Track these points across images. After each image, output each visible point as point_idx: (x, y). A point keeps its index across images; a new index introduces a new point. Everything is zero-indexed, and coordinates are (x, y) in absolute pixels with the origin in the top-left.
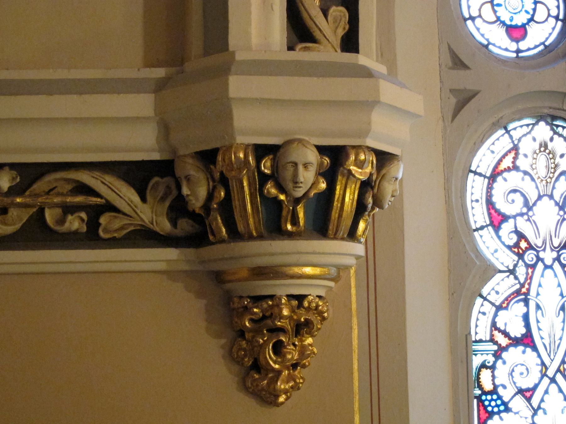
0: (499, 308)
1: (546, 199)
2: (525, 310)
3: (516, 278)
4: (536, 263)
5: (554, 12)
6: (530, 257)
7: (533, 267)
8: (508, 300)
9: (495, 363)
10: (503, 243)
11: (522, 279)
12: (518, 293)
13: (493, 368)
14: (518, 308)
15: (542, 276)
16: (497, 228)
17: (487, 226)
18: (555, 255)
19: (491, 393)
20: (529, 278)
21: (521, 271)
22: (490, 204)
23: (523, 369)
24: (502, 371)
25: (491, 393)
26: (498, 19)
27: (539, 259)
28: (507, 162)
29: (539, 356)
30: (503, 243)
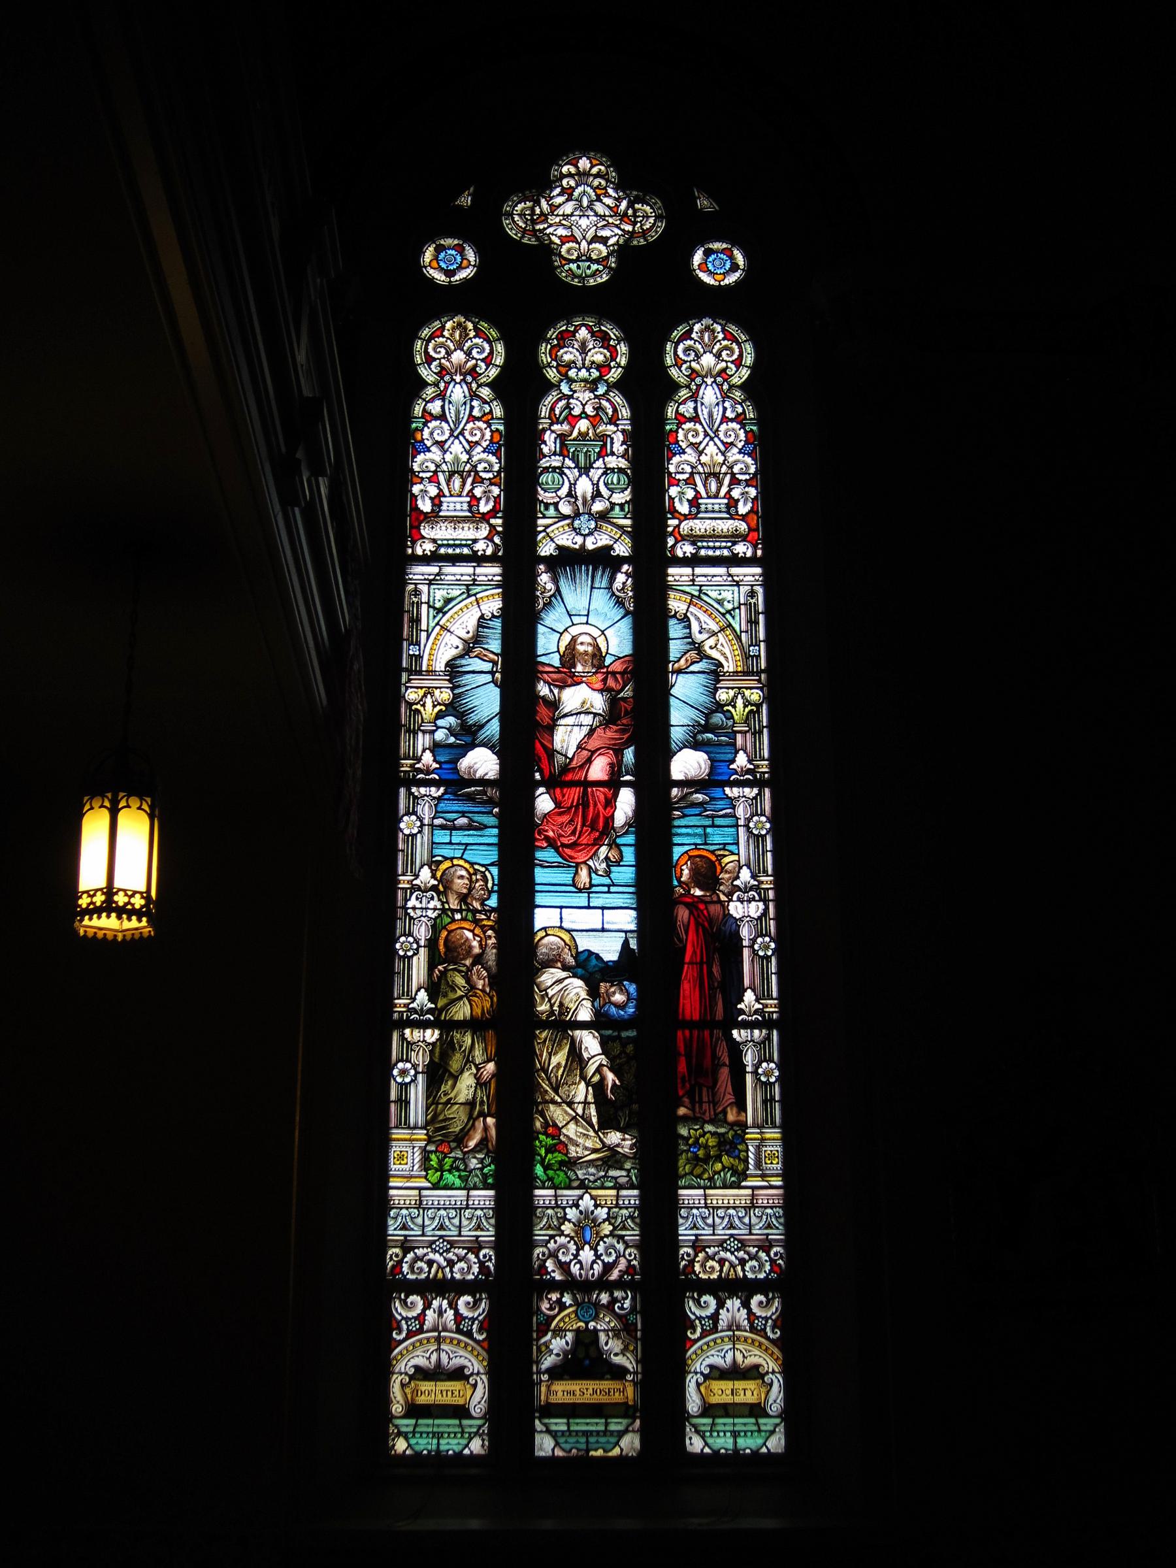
0: (680, 404)
1: (708, 353)
2: (442, 403)
3: (439, 388)
4: (701, 385)
5: (473, 263)
6: (447, 378)
7: (449, 383)
8: (686, 400)
9: (423, 428)
10: (432, 372)
11: (442, 389)
12: (691, 397)
13: (422, 430)
14: (691, 405)
15: (454, 387)
16: (429, 365)
17: (493, 364)
18: (713, 380)
19: (420, 442)
20: (446, 388)
21: (442, 385)
22: (426, 352)
23: (439, 432)
24: (426, 433)
25: (420, 442)
26: (440, 267)
27: (703, 381)
28: (438, 333)
29: (449, 426)
30: (432, 372)
